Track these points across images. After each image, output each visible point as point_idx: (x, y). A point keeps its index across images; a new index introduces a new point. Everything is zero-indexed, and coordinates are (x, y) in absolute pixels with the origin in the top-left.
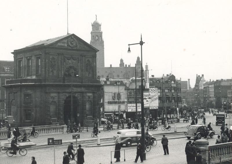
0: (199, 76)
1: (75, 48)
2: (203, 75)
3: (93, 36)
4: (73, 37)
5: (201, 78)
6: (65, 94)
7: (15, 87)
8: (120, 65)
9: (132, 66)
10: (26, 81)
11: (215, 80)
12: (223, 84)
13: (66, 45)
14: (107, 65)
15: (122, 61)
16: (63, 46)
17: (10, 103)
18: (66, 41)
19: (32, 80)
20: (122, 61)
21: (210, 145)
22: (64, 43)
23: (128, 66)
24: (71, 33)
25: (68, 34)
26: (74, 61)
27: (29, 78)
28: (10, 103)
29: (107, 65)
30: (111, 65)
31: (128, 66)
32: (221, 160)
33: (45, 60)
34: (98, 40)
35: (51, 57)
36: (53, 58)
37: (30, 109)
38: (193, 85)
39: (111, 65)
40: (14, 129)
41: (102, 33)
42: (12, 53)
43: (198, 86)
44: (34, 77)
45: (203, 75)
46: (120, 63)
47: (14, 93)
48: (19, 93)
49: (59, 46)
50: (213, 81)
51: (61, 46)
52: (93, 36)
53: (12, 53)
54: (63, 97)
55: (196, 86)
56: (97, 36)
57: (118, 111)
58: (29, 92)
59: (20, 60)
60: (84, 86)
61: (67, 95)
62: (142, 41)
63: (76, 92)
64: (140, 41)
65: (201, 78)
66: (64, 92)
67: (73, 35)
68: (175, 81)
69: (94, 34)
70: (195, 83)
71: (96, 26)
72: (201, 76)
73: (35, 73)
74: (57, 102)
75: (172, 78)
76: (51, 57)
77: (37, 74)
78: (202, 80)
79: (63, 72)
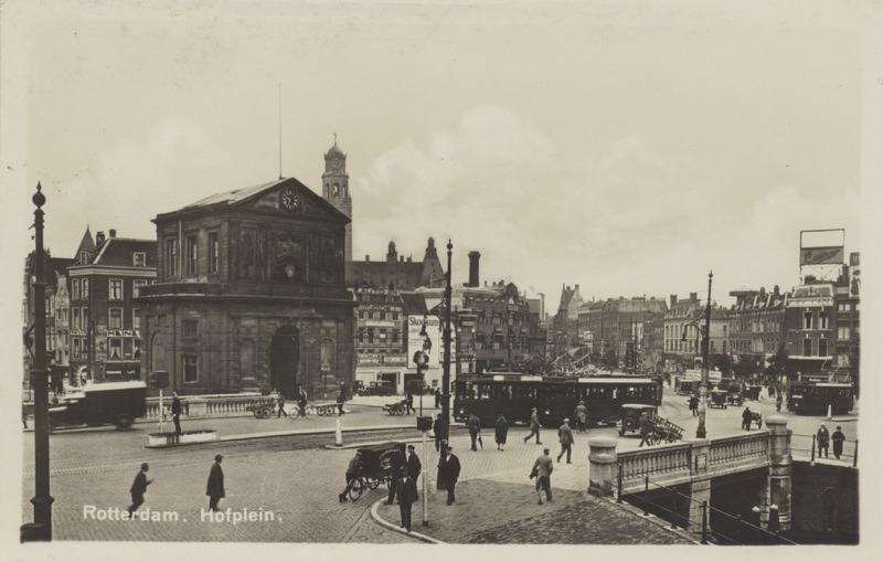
0: (568, 288)
1: (297, 213)
2: (577, 287)
3: (328, 185)
4: (292, 186)
5: (573, 292)
6: (273, 322)
7: (160, 301)
8: (388, 255)
9: (414, 260)
10: (185, 288)
11: (605, 300)
12: (622, 309)
13: (277, 206)
14: (358, 254)
15: (392, 246)
16: (269, 208)
17: (150, 337)
18: (276, 195)
19: (198, 287)
20: (392, 246)
21: (618, 450)
22: (272, 200)
23: (405, 260)
24: (287, 176)
25: (281, 178)
26: (295, 245)
27: (192, 281)
28: (150, 337)
29: (358, 254)
30: (367, 257)
31: (405, 260)
32: (650, 485)
33: (229, 241)
34: (337, 194)
35: (243, 233)
36: (248, 237)
37: (194, 354)
38: (551, 308)
39: (367, 257)
40: (471, 327)
41: (347, 177)
42: (152, 221)
43: (566, 310)
44: (204, 280)
45: (577, 287)
46: (427, 246)
47: (159, 316)
48: (169, 317)
49: (261, 207)
50: (601, 301)
51: (265, 207)
52: (328, 185)
53: (152, 221)
54: (272, 326)
55: (560, 310)
56: (337, 184)
57: (54, 442)
58: (194, 314)
59: (171, 238)
60: (316, 306)
61: (279, 324)
62: (46, 246)
63: (297, 319)
64: (32, 247)
65: (573, 292)
66: (273, 317)
67: (293, 181)
68: (516, 297)
69: (329, 180)
70: (559, 303)
71: (335, 159)
72: (573, 288)
73: (205, 270)
74: (256, 340)
75: (511, 291)
76: (243, 233)
77: (209, 271)
78: (575, 296)
79: (269, 271)
